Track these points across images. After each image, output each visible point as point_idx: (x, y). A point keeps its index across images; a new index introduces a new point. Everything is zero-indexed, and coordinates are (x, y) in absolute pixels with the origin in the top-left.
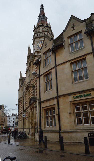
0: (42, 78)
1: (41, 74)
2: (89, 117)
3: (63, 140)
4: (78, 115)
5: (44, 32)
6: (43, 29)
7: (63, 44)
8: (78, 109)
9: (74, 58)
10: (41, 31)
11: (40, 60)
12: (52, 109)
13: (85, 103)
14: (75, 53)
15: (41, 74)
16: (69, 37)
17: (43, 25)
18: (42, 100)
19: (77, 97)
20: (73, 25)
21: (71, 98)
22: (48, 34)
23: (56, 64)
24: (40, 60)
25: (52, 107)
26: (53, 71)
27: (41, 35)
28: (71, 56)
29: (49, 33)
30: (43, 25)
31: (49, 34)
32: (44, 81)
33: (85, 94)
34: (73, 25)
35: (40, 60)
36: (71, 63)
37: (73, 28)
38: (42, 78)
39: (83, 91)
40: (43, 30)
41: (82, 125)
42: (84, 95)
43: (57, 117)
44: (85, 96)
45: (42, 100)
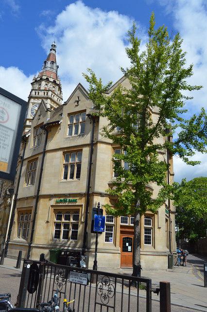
0: (26, 162)
1: (25, 157)
2: (113, 232)
3: (171, 289)
4: (58, 226)
5: (47, 90)
6: (46, 84)
7: (60, 123)
8: (59, 217)
9: (68, 146)
10: (42, 88)
11: (27, 136)
12: (28, 212)
13: (68, 211)
14: (71, 139)
15: (25, 157)
16: (69, 115)
17: (47, 79)
18: (18, 197)
19: (61, 201)
20: (78, 98)
21: (53, 202)
22: (52, 94)
23: (45, 149)
24: (27, 136)
25: (29, 209)
26: (40, 157)
27: (41, 94)
28: (66, 142)
29: (54, 93)
30: (47, 79)
31: (54, 96)
32: (27, 168)
33: (71, 199)
34: (78, 98)
35: (29, 136)
36: (64, 153)
37: (78, 102)
38: (26, 162)
39: (70, 195)
40: (46, 87)
41: (151, 245)
42: (69, 200)
43: (31, 224)
44: (70, 201)
45: (18, 197)
